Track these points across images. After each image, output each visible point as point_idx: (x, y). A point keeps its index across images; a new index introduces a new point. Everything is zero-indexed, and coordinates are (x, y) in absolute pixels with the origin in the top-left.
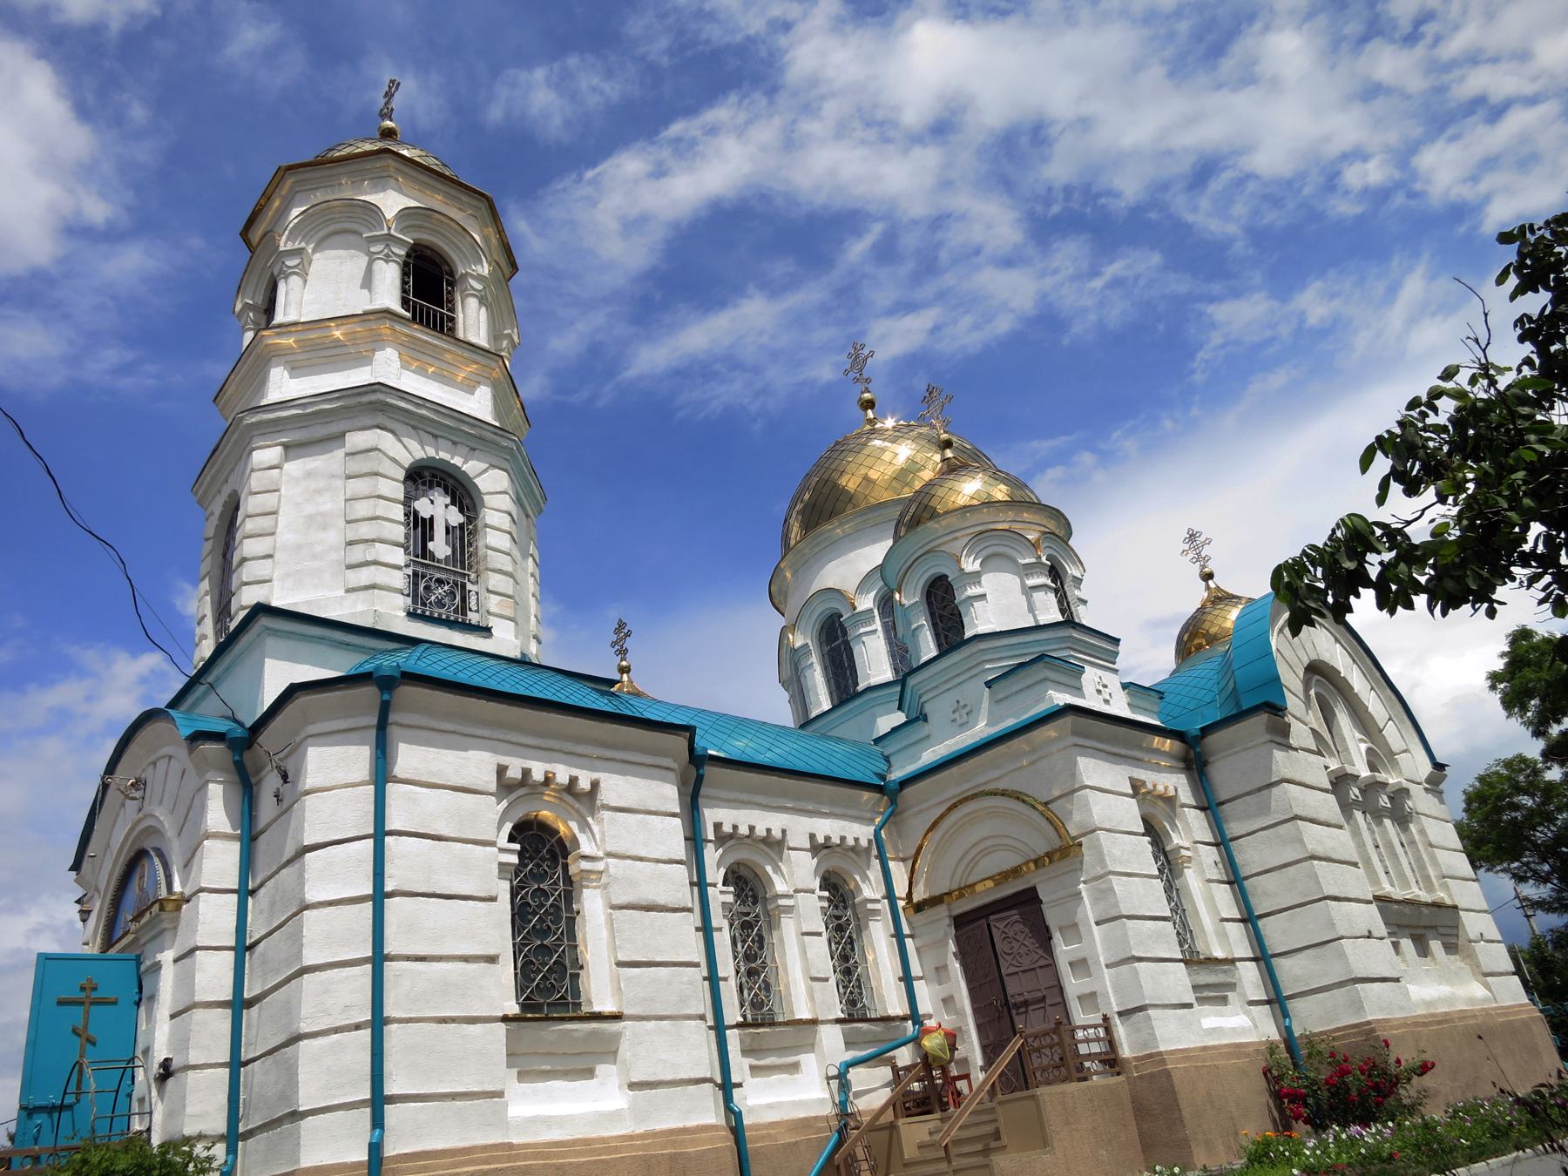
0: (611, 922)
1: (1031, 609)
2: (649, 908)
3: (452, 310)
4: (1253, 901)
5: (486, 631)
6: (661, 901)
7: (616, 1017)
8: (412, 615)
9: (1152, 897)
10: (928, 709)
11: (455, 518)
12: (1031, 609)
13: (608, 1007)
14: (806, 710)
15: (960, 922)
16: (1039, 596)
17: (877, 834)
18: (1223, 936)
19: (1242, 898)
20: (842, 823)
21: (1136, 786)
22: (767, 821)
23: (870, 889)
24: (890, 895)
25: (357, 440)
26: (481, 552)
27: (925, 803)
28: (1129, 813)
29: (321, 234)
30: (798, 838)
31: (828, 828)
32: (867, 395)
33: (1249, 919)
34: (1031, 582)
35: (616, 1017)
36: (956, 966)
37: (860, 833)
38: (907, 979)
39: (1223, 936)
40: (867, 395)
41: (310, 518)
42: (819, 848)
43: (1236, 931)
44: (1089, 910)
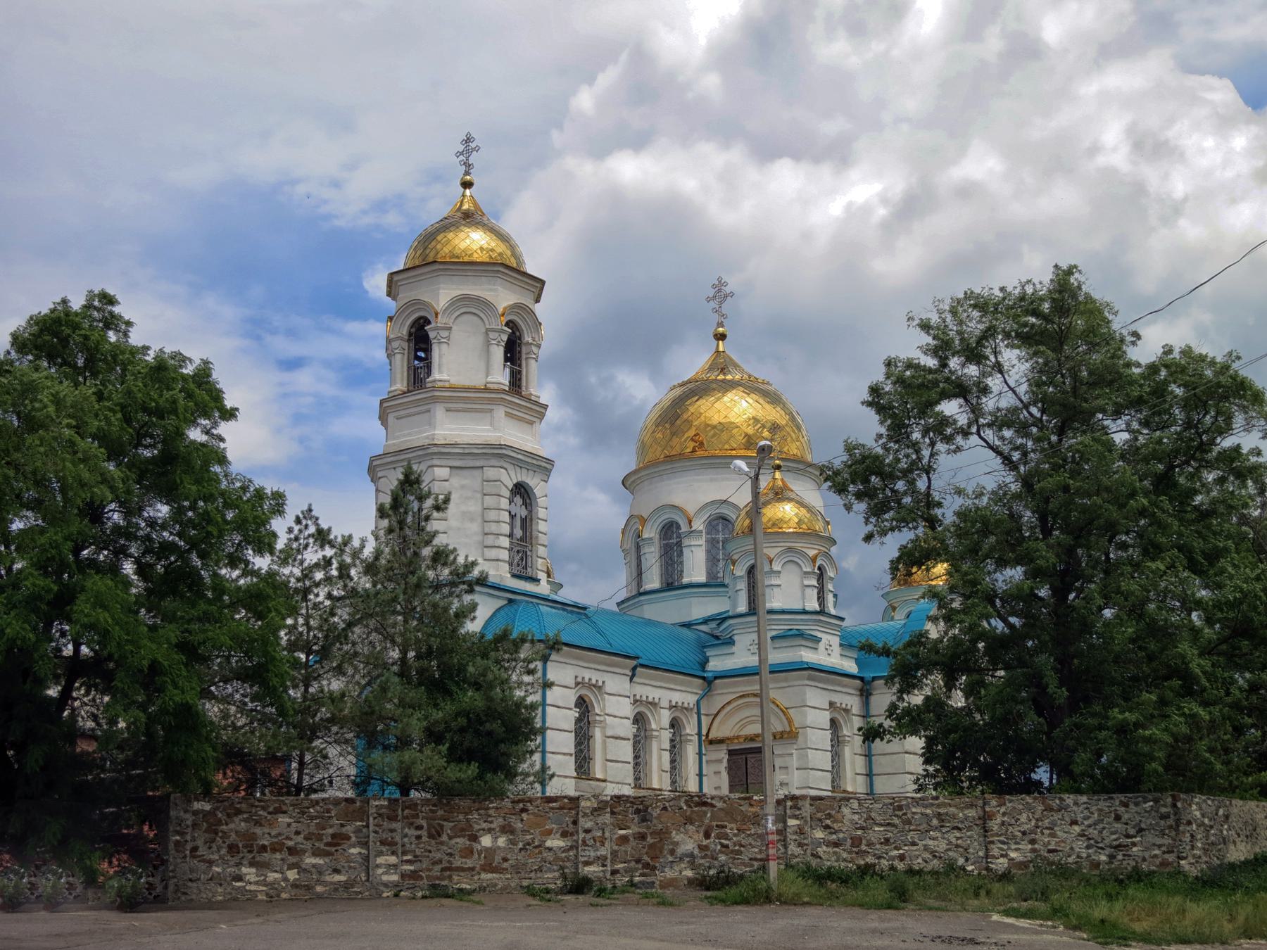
0: (604, 743)
1: (803, 598)
2: (617, 738)
3: (520, 366)
4: (874, 767)
5: (535, 580)
6: (622, 735)
7: (604, 781)
8: (514, 576)
9: (825, 760)
10: (735, 638)
11: (524, 513)
12: (803, 598)
13: (599, 776)
14: (639, 584)
15: (731, 753)
16: (808, 591)
17: (698, 702)
18: (854, 780)
19: (870, 764)
20: (684, 694)
21: (832, 704)
22: (653, 694)
23: (690, 729)
24: (699, 734)
25: (491, 473)
26: (535, 533)
27: (724, 693)
28: (824, 718)
29: (458, 313)
30: (665, 704)
31: (677, 697)
32: (721, 329)
33: (870, 775)
34: (806, 583)
35: (604, 781)
36: (725, 775)
37: (691, 700)
38: (700, 775)
39: (854, 780)
40: (721, 329)
41: (464, 513)
42: (672, 707)
43: (861, 779)
44: (794, 762)
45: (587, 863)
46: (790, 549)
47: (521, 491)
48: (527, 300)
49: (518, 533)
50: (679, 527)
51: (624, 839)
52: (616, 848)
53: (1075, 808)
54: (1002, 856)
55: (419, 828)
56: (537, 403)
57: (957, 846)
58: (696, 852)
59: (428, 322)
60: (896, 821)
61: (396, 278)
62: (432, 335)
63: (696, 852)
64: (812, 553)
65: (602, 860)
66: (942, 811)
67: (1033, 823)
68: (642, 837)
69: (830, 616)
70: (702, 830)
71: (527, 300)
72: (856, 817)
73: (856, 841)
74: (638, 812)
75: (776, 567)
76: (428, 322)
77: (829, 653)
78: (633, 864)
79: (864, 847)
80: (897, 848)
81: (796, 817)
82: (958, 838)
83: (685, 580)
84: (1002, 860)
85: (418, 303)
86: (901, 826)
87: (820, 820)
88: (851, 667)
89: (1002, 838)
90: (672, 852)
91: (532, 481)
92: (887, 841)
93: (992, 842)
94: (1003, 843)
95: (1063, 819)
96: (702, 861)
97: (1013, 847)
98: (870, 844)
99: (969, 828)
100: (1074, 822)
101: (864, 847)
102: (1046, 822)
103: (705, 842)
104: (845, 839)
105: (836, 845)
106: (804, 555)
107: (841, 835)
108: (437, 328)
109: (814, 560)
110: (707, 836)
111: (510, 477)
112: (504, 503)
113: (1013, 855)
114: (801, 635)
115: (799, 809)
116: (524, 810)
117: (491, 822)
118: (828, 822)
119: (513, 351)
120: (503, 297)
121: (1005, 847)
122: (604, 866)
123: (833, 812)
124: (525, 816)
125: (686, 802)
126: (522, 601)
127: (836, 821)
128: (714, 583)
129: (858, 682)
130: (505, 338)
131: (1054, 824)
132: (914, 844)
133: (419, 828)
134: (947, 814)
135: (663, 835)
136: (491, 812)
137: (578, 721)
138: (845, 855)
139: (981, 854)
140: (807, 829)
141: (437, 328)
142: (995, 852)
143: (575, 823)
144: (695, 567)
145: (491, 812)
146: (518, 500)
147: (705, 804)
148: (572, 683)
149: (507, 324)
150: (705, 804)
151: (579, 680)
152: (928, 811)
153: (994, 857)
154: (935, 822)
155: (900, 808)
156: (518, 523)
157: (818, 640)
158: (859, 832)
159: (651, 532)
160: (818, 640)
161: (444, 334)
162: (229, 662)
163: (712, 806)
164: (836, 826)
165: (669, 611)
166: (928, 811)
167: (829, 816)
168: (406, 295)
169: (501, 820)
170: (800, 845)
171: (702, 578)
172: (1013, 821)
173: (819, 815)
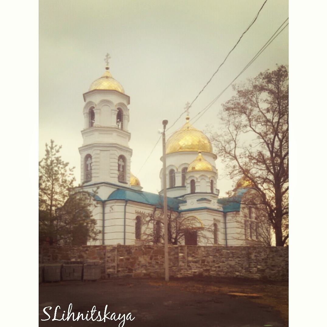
8: (120, 182)
10: (187, 201)
21: (214, 219)
25: (111, 152)
29: (103, 105)
45: (109, 268)
46: (203, 175)
47: (122, 157)
48: (125, 103)
49: (121, 169)
50: (174, 171)
51: (122, 260)
52: (119, 263)
53: (281, 251)
54: (255, 267)
55: (49, 256)
56: (128, 133)
57: (239, 263)
58: (147, 264)
59: (94, 108)
60: (217, 254)
61: (85, 95)
62: (95, 111)
63: (147, 264)
64: (209, 176)
65: (113, 267)
66: (234, 251)
67: (266, 256)
68: (128, 259)
69: (214, 194)
70: (150, 257)
71: (125, 103)
72: (203, 253)
73: (203, 261)
74: (127, 251)
75: (199, 180)
76: (94, 108)
77: (214, 205)
78: (125, 269)
79: (206, 263)
80: (217, 264)
81: (182, 253)
82: (239, 261)
83: (176, 186)
84: (254, 269)
85: (90, 103)
86: (219, 256)
87: (191, 254)
88: (221, 209)
89: (255, 261)
90: (139, 264)
91: (126, 155)
92: (214, 261)
93: (251, 262)
94: (255, 263)
95: (277, 255)
96: (149, 268)
97: (259, 264)
98: (208, 262)
99: (243, 258)
100: (281, 256)
101: (206, 263)
102: (271, 256)
103: (150, 261)
104: (199, 261)
105: (196, 262)
106: (207, 177)
107: (198, 259)
108: (97, 109)
109: (210, 178)
110: (151, 259)
111: (119, 153)
112: (117, 161)
113: (259, 267)
114: (205, 199)
115: (183, 250)
116: (87, 250)
117: (75, 254)
118: (193, 255)
119: (120, 116)
120: (116, 100)
121: (256, 264)
122: (114, 269)
123: (195, 251)
124: (87, 252)
125: (144, 248)
126: (122, 189)
127: (196, 254)
128: (183, 186)
129: (222, 213)
130: (117, 112)
131: (273, 256)
132: (223, 262)
133: (49, 256)
134: (235, 252)
135: (135, 259)
136: (75, 251)
137: (136, 224)
138: (199, 266)
139: (247, 266)
140: (186, 257)
141: (97, 109)
142: (252, 266)
143: (105, 254)
144: (178, 182)
145: (75, 251)
146: (121, 160)
147: (150, 248)
148: (134, 212)
149: (118, 109)
150: (150, 248)
151: (137, 211)
152: (229, 251)
153: (252, 267)
154: (231, 255)
155: (219, 250)
156: (121, 167)
157: (211, 201)
158: (204, 258)
159: (167, 172)
160: (211, 201)
161: (98, 111)
162: (248, 240)
163: (153, 249)
164: (196, 256)
165: (172, 194)
166: (229, 251)
167: (194, 253)
168: (88, 100)
169: (79, 254)
170: (183, 262)
171: (180, 185)
172: (259, 255)
173: (190, 252)
